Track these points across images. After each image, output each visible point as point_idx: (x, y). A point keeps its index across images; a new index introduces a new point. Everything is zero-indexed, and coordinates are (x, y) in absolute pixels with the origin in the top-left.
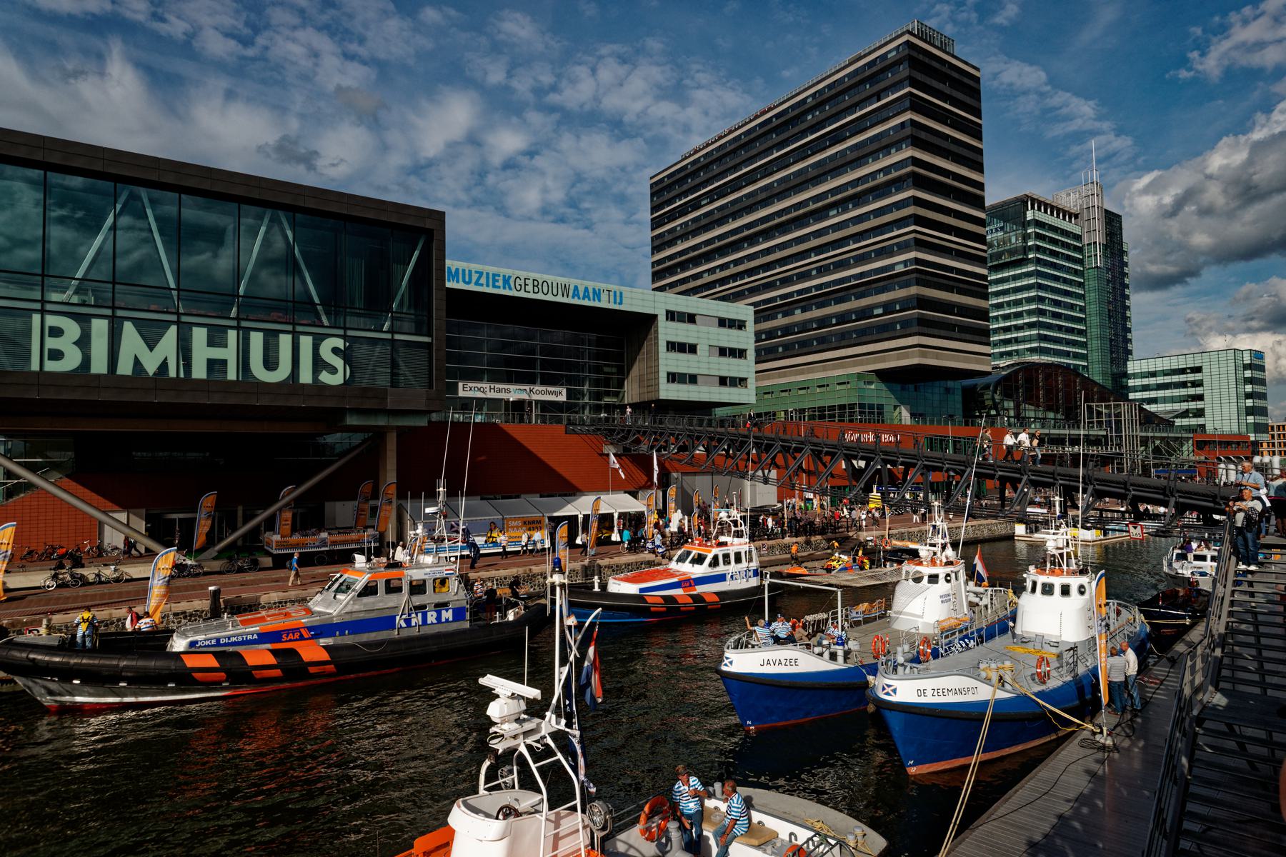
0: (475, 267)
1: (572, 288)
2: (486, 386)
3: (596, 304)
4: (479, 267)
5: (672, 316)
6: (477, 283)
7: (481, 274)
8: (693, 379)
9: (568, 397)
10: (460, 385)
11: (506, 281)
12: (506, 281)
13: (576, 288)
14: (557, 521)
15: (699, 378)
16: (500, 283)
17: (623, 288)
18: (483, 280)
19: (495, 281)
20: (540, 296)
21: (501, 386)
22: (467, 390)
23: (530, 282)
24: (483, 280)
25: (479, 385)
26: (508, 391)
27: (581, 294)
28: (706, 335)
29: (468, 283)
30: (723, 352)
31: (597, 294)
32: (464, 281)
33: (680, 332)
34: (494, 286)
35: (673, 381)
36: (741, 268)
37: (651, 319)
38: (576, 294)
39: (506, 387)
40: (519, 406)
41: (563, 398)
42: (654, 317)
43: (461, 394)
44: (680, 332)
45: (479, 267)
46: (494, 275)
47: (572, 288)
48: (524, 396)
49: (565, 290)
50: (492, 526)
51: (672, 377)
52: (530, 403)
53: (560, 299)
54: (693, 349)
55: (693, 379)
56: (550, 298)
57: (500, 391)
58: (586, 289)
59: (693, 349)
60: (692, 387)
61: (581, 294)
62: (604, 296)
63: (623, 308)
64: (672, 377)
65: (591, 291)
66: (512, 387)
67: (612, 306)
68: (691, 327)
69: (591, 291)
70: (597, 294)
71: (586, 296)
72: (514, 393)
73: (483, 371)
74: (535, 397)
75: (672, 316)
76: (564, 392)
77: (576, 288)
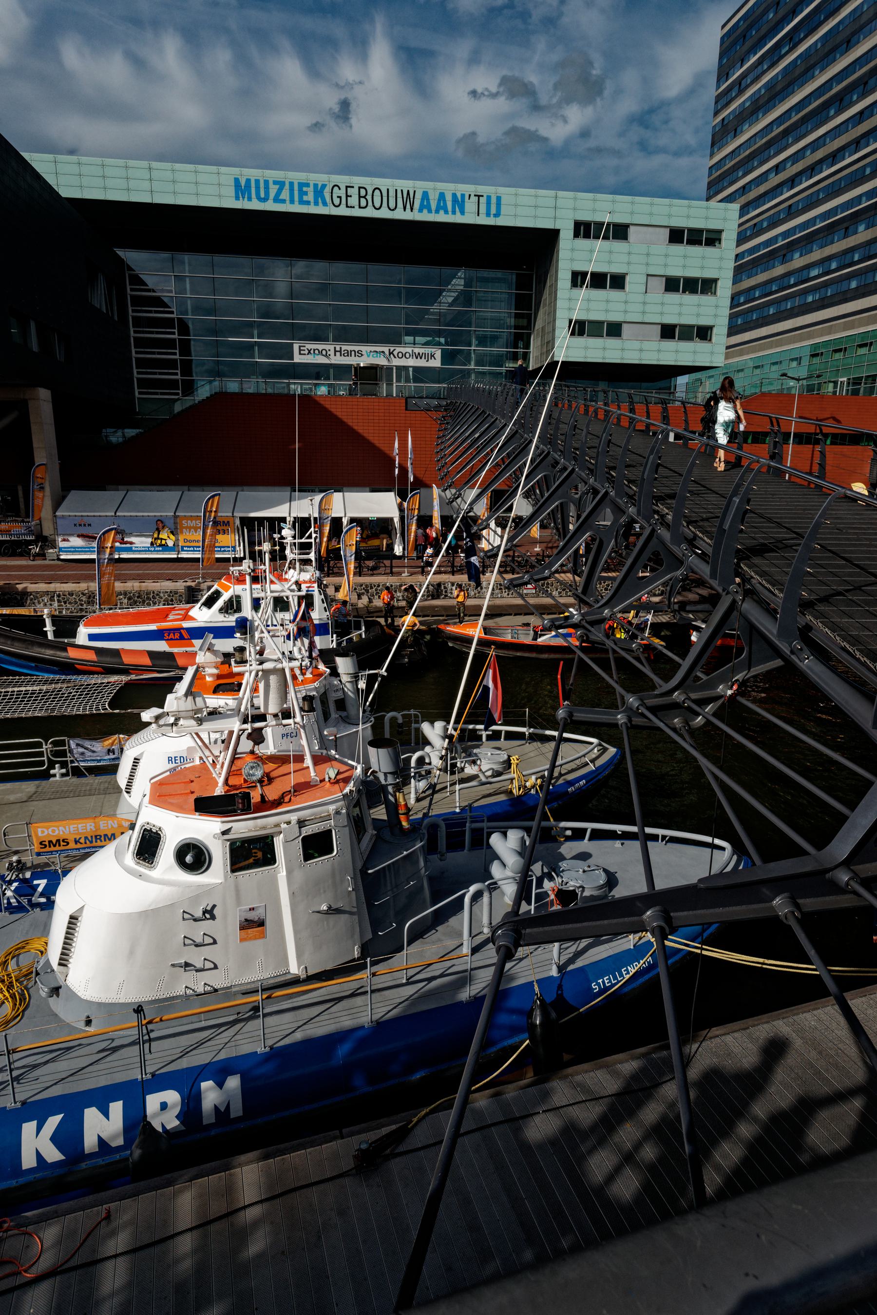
0: (272, 175)
1: (419, 196)
2: (330, 347)
3: (458, 219)
4: (278, 175)
5: (584, 230)
6: (277, 200)
7: (281, 184)
8: (614, 330)
9: (444, 361)
10: (296, 347)
11: (319, 192)
12: (319, 192)
13: (425, 195)
14: (248, 523)
15: (625, 328)
16: (310, 197)
17: (501, 190)
18: (285, 195)
19: (302, 193)
20: (369, 213)
21: (349, 348)
22: (305, 353)
23: (354, 192)
24: (285, 195)
25: (320, 346)
26: (359, 354)
27: (433, 206)
28: (644, 257)
29: (265, 200)
30: (672, 285)
31: (459, 203)
32: (259, 199)
33: (596, 256)
34: (302, 202)
35: (581, 333)
36: (820, 154)
37: (548, 239)
38: (425, 206)
39: (357, 348)
40: (370, 375)
41: (436, 363)
42: (553, 235)
43: (298, 359)
44: (596, 256)
45: (278, 175)
46: (301, 185)
47: (419, 196)
48: (382, 361)
49: (408, 200)
50: (160, 525)
51: (579, 328)
52: (389, 369)
53: (400, 214)
54: (618, 282)
55: (614, 330)
56: (384, 214)
57: (349, 354)
58: (442, 196)
59: (618, 282)
60: (612, 342)
61: (433, 206)
62: (470, 205)
63: (501, 222)
64: (579, 328)
65: (449, 198)
66: (365, 349)
67: (483, 220)
68: (618, 246)
69: (449, 198)
70: (459, 203)
71: (441, 206)
72: (368, 355)
73: (251, 325)
74: (396, 362)
75: (584, 230)
76: (438, 354)
77: (425, 195)
